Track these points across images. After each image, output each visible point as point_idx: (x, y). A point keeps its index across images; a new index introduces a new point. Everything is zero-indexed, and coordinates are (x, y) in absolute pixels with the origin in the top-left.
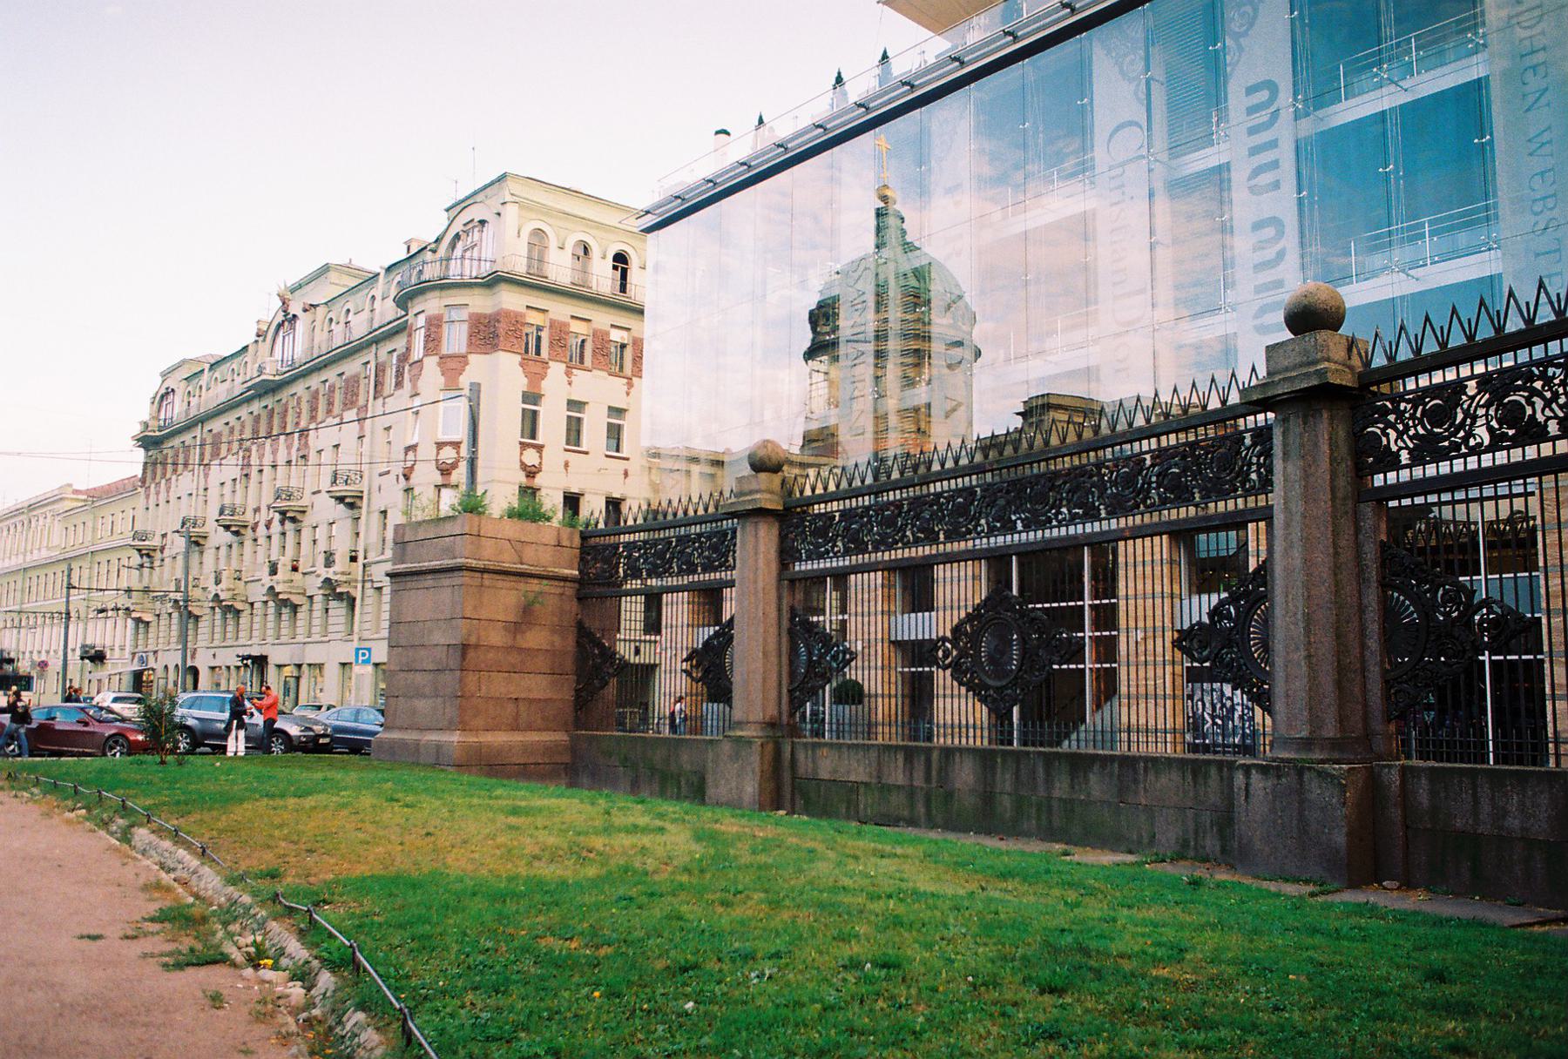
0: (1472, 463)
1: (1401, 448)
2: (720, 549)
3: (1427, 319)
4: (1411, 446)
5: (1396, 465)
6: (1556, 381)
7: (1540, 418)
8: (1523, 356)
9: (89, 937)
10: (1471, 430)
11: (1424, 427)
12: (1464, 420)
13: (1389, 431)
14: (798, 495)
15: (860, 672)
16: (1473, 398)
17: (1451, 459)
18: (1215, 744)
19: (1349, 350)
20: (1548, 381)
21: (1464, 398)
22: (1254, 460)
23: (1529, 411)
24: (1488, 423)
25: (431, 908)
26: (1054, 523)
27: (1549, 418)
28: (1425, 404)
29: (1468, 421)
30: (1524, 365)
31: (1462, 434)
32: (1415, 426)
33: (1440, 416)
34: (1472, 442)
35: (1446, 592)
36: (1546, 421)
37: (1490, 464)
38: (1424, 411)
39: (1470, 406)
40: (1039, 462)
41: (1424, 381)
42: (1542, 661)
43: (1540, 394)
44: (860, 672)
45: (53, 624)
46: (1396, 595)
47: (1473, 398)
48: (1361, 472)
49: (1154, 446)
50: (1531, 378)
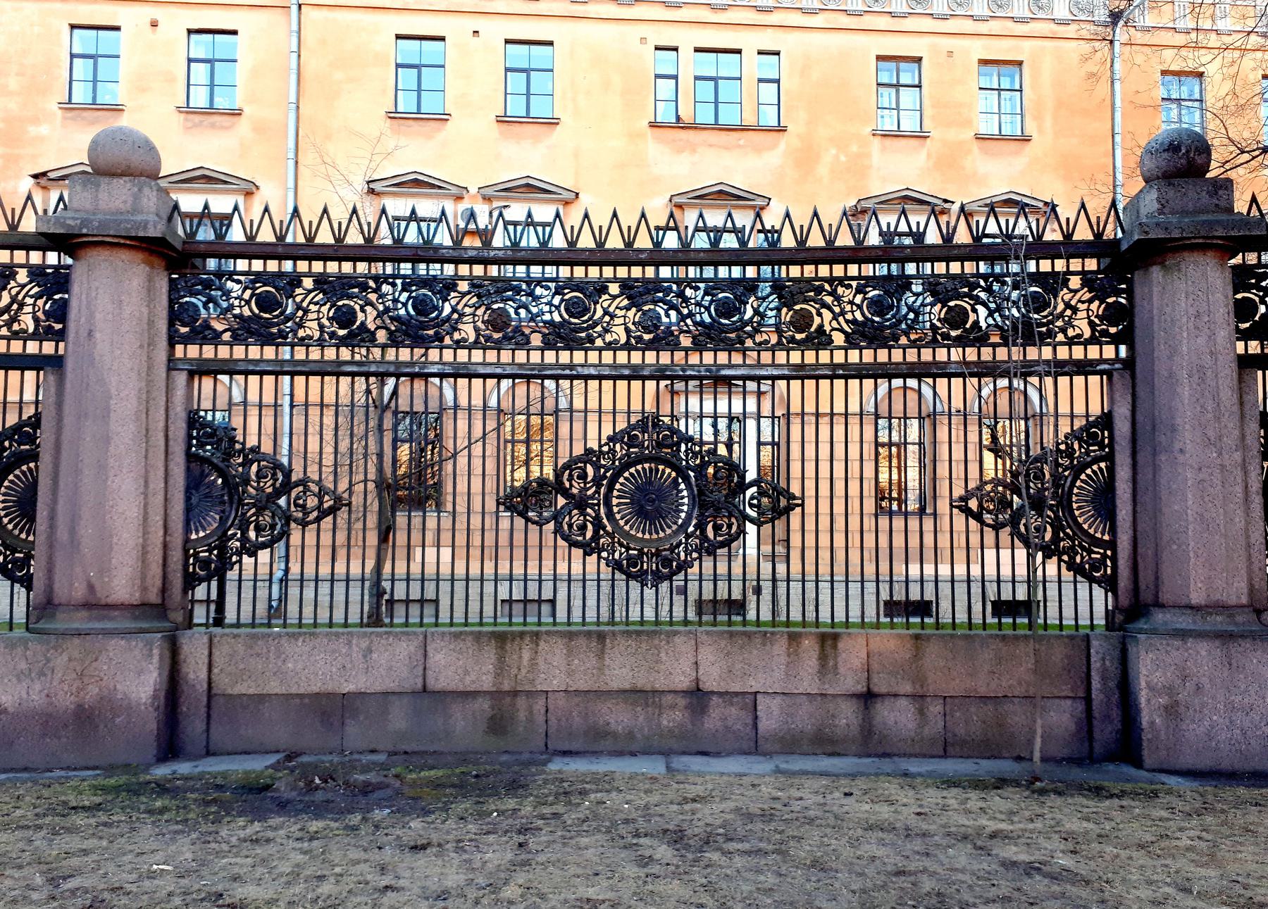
0: (300, 353)
3: (615, 215)
16: (23, 286)
24: (34, 313)
25: (1154, 866)
27: (834, 329)
28: (254, 289)
29: (15, 306)
30: (362, 276)
31: (599, 329)
36: (376, 329)
38: (864, 299)
39: (18, 293)
42: (886, 616)
43: (372, 304)
47: (23, 286)
49: (929, 271)
50: (819, 290)
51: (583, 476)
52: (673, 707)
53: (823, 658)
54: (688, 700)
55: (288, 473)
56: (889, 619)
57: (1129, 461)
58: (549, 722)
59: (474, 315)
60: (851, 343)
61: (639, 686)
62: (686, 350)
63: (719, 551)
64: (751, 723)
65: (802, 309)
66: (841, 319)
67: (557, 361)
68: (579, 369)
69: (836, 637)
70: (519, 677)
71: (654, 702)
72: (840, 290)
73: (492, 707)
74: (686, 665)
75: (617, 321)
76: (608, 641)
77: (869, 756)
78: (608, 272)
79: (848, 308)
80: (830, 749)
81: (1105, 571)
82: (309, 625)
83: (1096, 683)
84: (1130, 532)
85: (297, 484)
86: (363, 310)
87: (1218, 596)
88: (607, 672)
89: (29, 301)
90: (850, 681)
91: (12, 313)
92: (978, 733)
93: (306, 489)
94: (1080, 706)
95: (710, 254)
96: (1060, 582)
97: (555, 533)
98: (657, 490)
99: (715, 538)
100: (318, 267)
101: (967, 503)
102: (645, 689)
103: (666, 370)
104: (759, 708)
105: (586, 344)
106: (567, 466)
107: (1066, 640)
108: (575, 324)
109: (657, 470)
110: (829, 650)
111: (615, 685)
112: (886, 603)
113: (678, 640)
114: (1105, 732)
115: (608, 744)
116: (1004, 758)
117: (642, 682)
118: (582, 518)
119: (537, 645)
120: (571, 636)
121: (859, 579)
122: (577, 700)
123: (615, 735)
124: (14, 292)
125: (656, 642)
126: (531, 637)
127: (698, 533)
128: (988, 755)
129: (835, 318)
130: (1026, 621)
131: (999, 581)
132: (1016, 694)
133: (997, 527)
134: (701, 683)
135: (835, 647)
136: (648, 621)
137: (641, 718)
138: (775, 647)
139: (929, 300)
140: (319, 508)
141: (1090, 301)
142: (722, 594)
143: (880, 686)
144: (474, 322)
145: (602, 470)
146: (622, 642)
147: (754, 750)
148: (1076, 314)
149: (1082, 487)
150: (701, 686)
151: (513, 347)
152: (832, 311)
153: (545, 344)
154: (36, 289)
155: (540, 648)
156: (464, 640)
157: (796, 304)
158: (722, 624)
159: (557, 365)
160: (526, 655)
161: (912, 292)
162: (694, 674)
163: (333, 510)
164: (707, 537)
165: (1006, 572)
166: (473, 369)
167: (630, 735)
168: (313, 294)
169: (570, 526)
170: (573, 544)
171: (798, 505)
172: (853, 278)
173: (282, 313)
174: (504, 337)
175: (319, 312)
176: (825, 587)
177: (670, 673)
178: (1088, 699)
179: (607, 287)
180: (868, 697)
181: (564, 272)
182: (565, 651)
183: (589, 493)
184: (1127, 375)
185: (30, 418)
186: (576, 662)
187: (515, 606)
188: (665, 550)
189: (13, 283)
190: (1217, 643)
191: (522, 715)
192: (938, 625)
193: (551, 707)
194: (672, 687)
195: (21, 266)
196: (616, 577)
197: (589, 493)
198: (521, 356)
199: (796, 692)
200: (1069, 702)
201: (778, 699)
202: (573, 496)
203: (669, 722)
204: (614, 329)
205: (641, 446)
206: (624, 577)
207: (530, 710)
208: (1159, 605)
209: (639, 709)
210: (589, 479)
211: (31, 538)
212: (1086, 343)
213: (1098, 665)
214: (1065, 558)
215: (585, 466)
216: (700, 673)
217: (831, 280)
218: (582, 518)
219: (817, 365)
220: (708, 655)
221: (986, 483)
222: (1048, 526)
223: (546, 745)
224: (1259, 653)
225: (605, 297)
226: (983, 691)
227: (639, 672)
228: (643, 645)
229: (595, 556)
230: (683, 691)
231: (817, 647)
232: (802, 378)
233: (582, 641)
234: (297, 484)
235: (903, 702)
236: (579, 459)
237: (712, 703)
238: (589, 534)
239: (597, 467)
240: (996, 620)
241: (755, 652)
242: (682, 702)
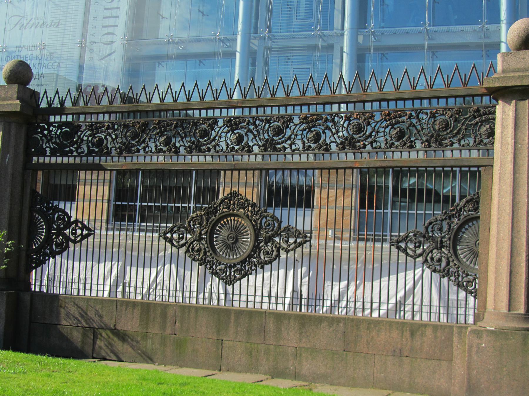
1: (47, 147)
2: (418, 110)
3: (57, 92)
4: (52, 147)
5: (44, 155)
7: (109, 146)
9: (204, 377)
10: (80, 145)
11: (60, 139)
12: (77, 140)
13: (326, 131)
16: (296, 125)
19: (31, 96)
20: (256, 126)
21: (292, 124)
22: (300, 133)
23: (41, 143)
28: (62, 129)
32: (56, 138)
34: (79, 150)
35: (59, 216)
37: (73, 162)
39: (219, 131)
40: (250, 107)
43: (251, 132)
45: (300, 10)
46: (37, 215)
48: (28, 156)
55: (70, 217)
59: (384, 132)
63: (266, 266)
86: (324, 132)
89: (382, 130)
91: (216, 141)
99: (56, 249)
124: (293, 128)
128: (129, 361)
133: (415, 257)
140: (295, 242)
144: (226, 140)
154: (89, 132)
163: (87, 236)
168: (223, 128)
169: (432, 259)
171: (92, 234)
173: (209, 139)
175: (384, 132)
185: (228, 195)
189: (292, 124)
195: (377, 111)
210: (444, 231)
211: (476, 267)
212: (87, 155)
238: (444, 264)
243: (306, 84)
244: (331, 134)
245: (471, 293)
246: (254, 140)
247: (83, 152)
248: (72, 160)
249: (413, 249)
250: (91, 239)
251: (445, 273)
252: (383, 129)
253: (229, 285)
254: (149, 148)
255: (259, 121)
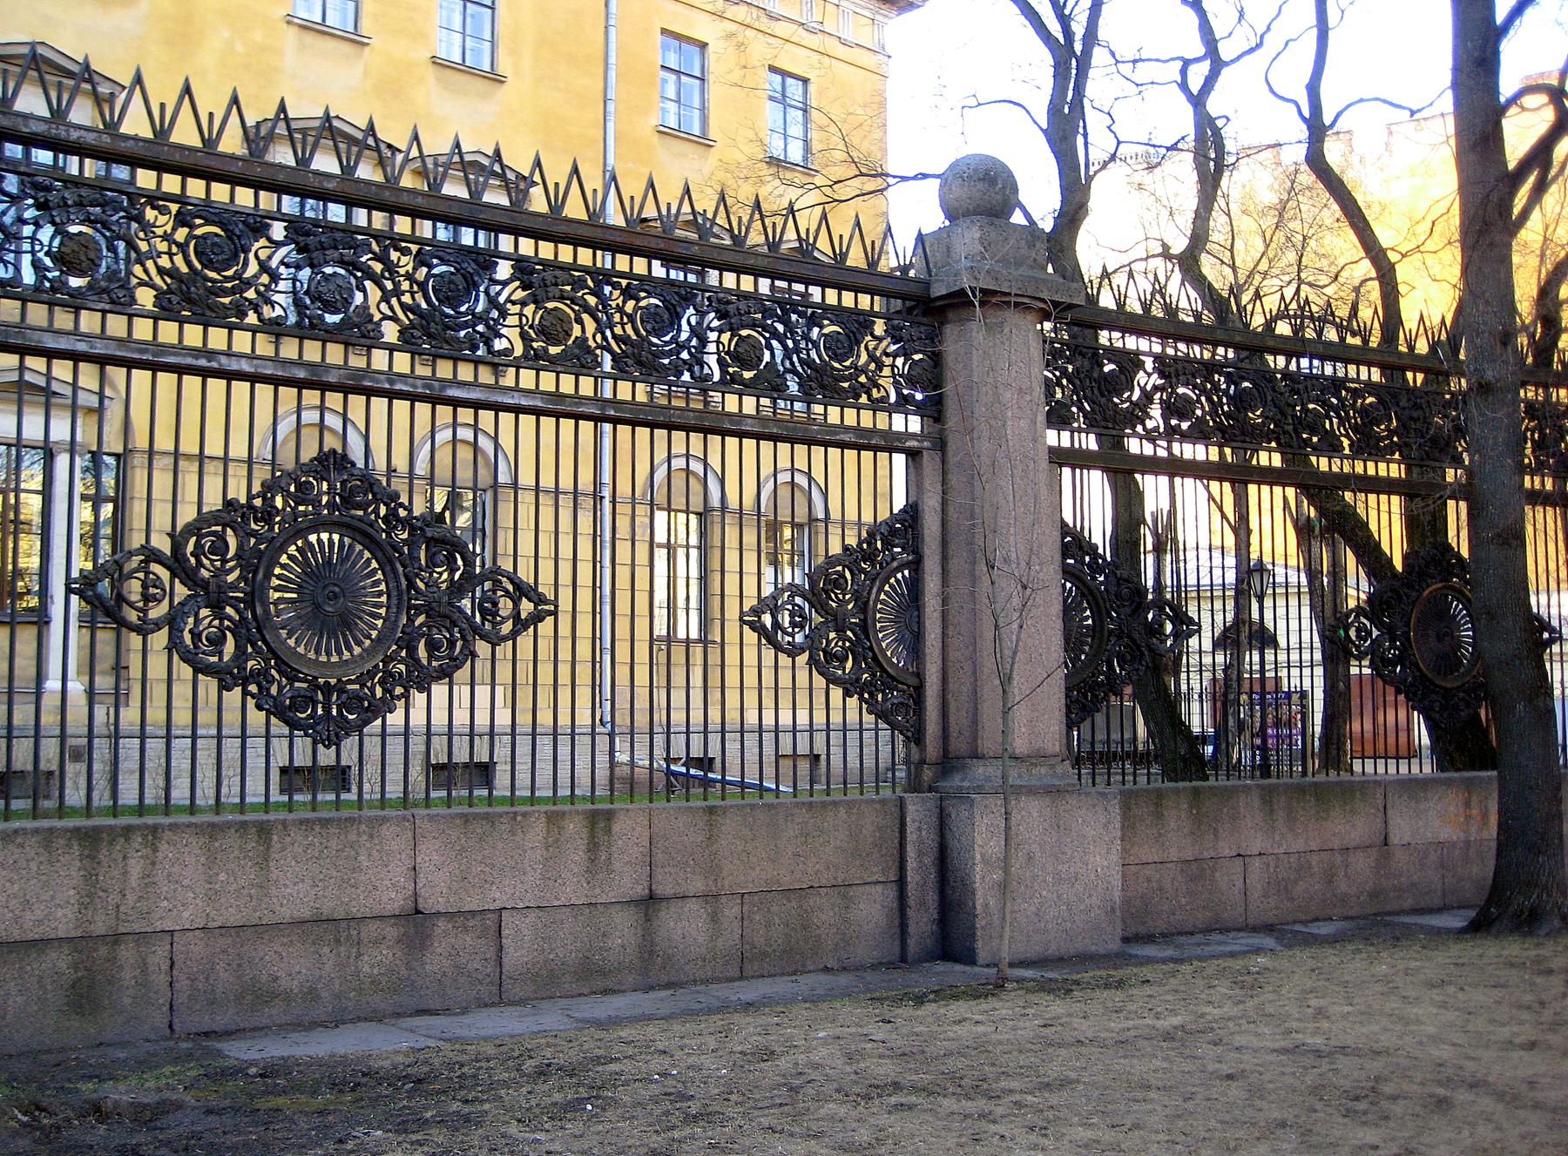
6: (402, 271)
8: (566, 253)
14: (1403, 349)
15: (207, 717)
17: (231, 328)
18: (529, 1145)
23: (767, 357)
26: (864, 399)
27: (386, 318)
33: (455, 291)
41: (832, 297)
42: (282, 791)
44: (207, 717)
51: (220, 548)
52: (377, 942)
53: (593, 847)
54: (402, 930)
56: (286, 798)
57: (938, 569)
58: (177, 986)
59: (521, 315)
60: (408, 341)
61: (326, 912)
62: (391, 349)
64: (494, 957)
65: (556, 309)
66: (394, 301)
67: (181, 340)
68: (224, 360)
69: (609, 815)
70: (122, 909)
71: (349, 937)
72: (150, 214)
73: (76, 967)
74: (397, 872)
75: (282, 286)
76: (275, 838)
77: (649, 988)
78: (267, 200)
79: (405, 285)
80: (600, 984)
81: (314, 710)
82: (584, 798)
83: (911, 864)
84: (939, 662)
85: (483, 578)
87: (1039, 744)
88: (274, 892)
90: (627, 882)
92: (780, 941)
93: (497, 583)
94: (892, 892)
95: (625, 235)
96: (268, 736)
97: (169, 649)
98: (343, 580)
99: (429, 662)
100: (526, 246)
101: (760, 617)
102: (335, 916)
103: (363, 378)
104: (505, 932)
105: (229, 319)
106: (194, 529)
107: (878, 806)
108: (214, 281)
109: (311, 545)
110: (602, 838)
111: (286, 913)
112: (283, 771)
113: (387, 831)
114: (922, 923)
115: (275, 1012)
116: (810, 972)
117: (328, 907)
118: (216, 622)
119: (155, 850)
120: (213, 830)
121: (239, 733)
122: (222, 942)
123: (287, 996)
125: (353, 837)
126: (144, 837)
127: (403, 654)
129: (386, 298)
130: (485, 792)
131: (429, 734)
132: (824, 882)
134: (420, 900)
135: (609, 831)
136: (72, 808)
137: (328, 967)
138: (529, 836)
139: (30, 214)
141: (523, 304)
142: (461, 756)
143: (665, 888)
145: (253, 541)
146: (296, 835)
147: (496, 999)
148: (881, 371)
149: (884, 599)
150: (421, 907)
151: (107, 307)
152: (382, 288)
153: (163, 308)
155: (160, 854)
156: (21, 846)
157: (549, 299)
158: (20, 815)
159: (180, 348)
160: (136, 867)
161: (872, 335)
162: (412, 887)
163: (537, 618)
164: (418, 661)
165: (482, 720)
166: (34, 339)
167: (311, 994)
169: (196, 636)
170: (208, 670)
171: (550, 613)
172: (622, 275)
174: (90, 286)
176: (181, 746)
177: (375, 888)
178: (901, 882)
179: (268, 226)
180: (650, 902)
181: (196, 188)
182: (202, 859)
183: (231, 578)
184: (937, 457)
186: (222, 876)
187: (1394, 754)
188: (350, 682)
190: (1047, 801)
191: (128, 976)
192: (490, 800)
193: (178, 958)
194: (377, 911)
196: (273, 730)
197: (231, 578)
198: (116, 325)
199: (556, 903)
200: (879, 888)
201: (532, 916)
202: (205, 584)
203: (372, 966)
204: (504, 331)
205: (316, 503)
206: (286, 731)
207: (144, 967)
208: (976, 755)
209: (326, 950)
210: (231, 553)
212: (891, 410)
213: (915, 836)
214: (253, 688)
215: (224, 531)
216: (420, 885)
217: (592, 271)
218: (216, 622)
219: (577, 397)
220: (431, 854)
221: (783, 590)
222: (228, 634)
223: (170, 1027)
224: (1084, 811)
225: (263, 242)
226: (787, 882)
227: (325, 888)
228: (333, 843)
229: (238, 690)
230: (394, 916)
231: (585, 833)
232: (558, 415)
233: (231, 839)
234: (483, 578)
235: (692, 905)
236: (215, 517)
237: (438, 931)
239: (244, 534)
240: (286, 798)
241: (500, 845)
242: (391, 932)
243: (745, 220)
244: (379, 293)
245: (304, 728)
246: (384, 306)
247: (885, 399)
248: (850, 417)
249: (141, 604)
250: (546, 627)
251: (227, 678)
252: (716, 334)
253: (328, 747)
254: (879, 391)
255: (610, 288)
